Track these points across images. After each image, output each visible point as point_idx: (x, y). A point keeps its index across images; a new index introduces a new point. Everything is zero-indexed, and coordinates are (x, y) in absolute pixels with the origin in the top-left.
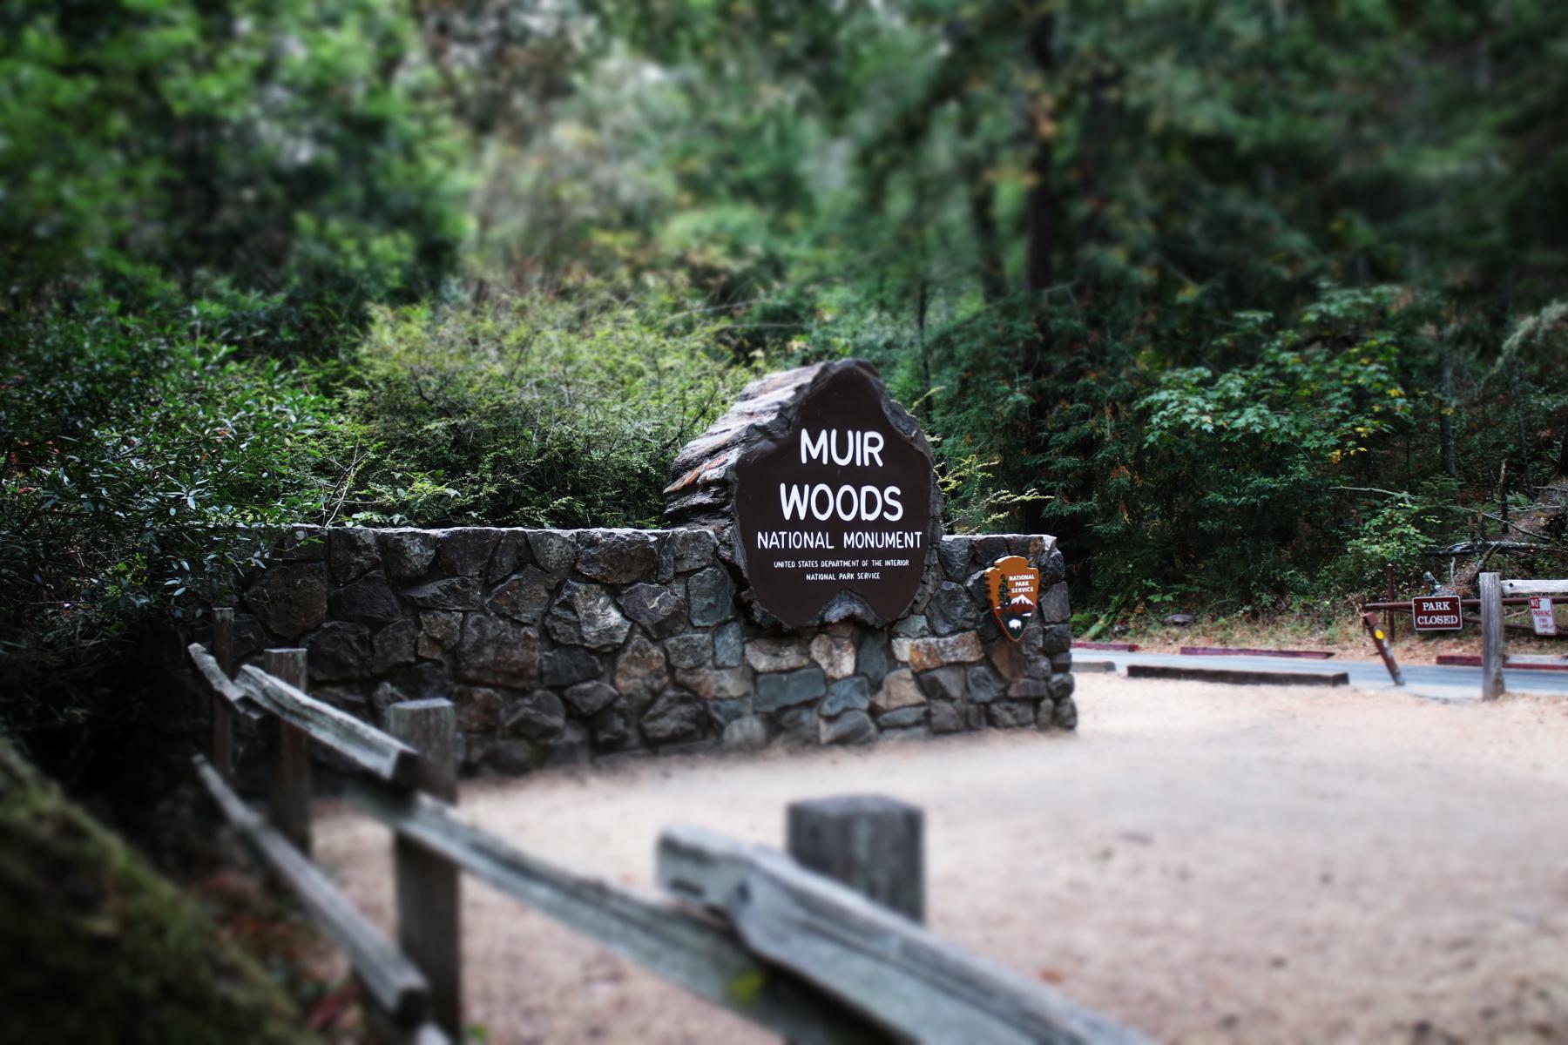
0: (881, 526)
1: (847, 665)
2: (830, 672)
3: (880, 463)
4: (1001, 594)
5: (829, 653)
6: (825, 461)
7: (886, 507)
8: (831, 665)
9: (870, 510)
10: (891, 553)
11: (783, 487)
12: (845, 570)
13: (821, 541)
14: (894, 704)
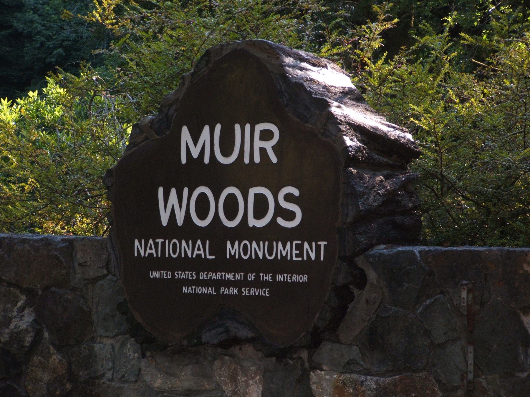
0: (272, 233)
7: (279, 211)
9: (259, 214)
12: (228, 284)
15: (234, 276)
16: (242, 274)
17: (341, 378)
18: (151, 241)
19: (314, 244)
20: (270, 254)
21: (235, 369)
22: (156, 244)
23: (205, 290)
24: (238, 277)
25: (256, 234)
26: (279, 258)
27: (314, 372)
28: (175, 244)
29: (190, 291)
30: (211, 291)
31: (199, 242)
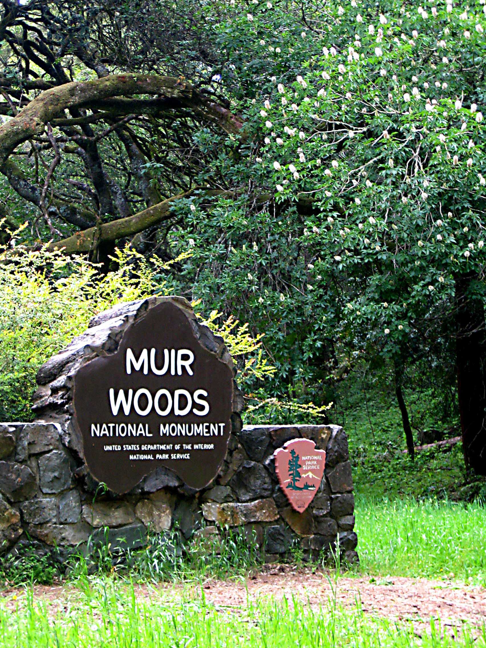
0: (191, 419)
3: (191, 373)
7: (195, 405)
10: (199, 439)
12: (162, 452)
13: (142, 430)
22: (109, 428)
23: (145, 457)
24: (168, 447)
25: (180, 420)
26: (195, 434)
29: (135, 457)
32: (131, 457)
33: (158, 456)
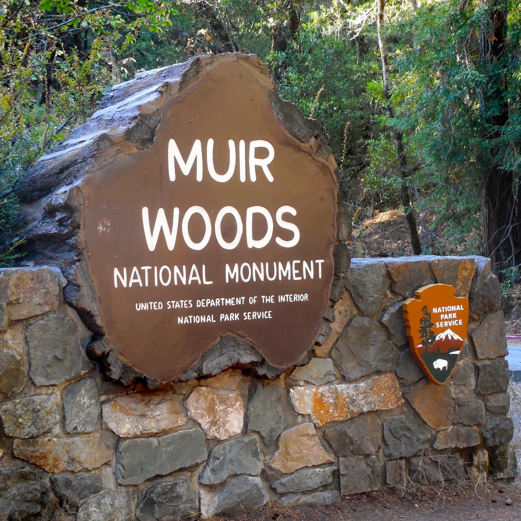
0: (273, 254)
1: (234, 422)
2: (213, 433)
4: (423, 330)
5: (211, 410)
6: (199, 177)
7: (279, 232)
8: (214, 423)
9: (258, 235)
10: (285, 286)
11: (145, 211)
12: (228, 310)
14: (293, 465)
15: (235, 300)
16: (243, 298)
17: (319, 391)
18: (135, 269)
19: (312, 262)
20: (271, 276)
21: (213, 400)
22: (142, 273)
23: (203, 319)
24: (238, 302)
25: (256, 256)
27: (294, 389)
28: (165, 272)
29: (186, 321)
30: (210, 319)
31: (194, 267)
32: (180, 321)
33: (222, 317)
